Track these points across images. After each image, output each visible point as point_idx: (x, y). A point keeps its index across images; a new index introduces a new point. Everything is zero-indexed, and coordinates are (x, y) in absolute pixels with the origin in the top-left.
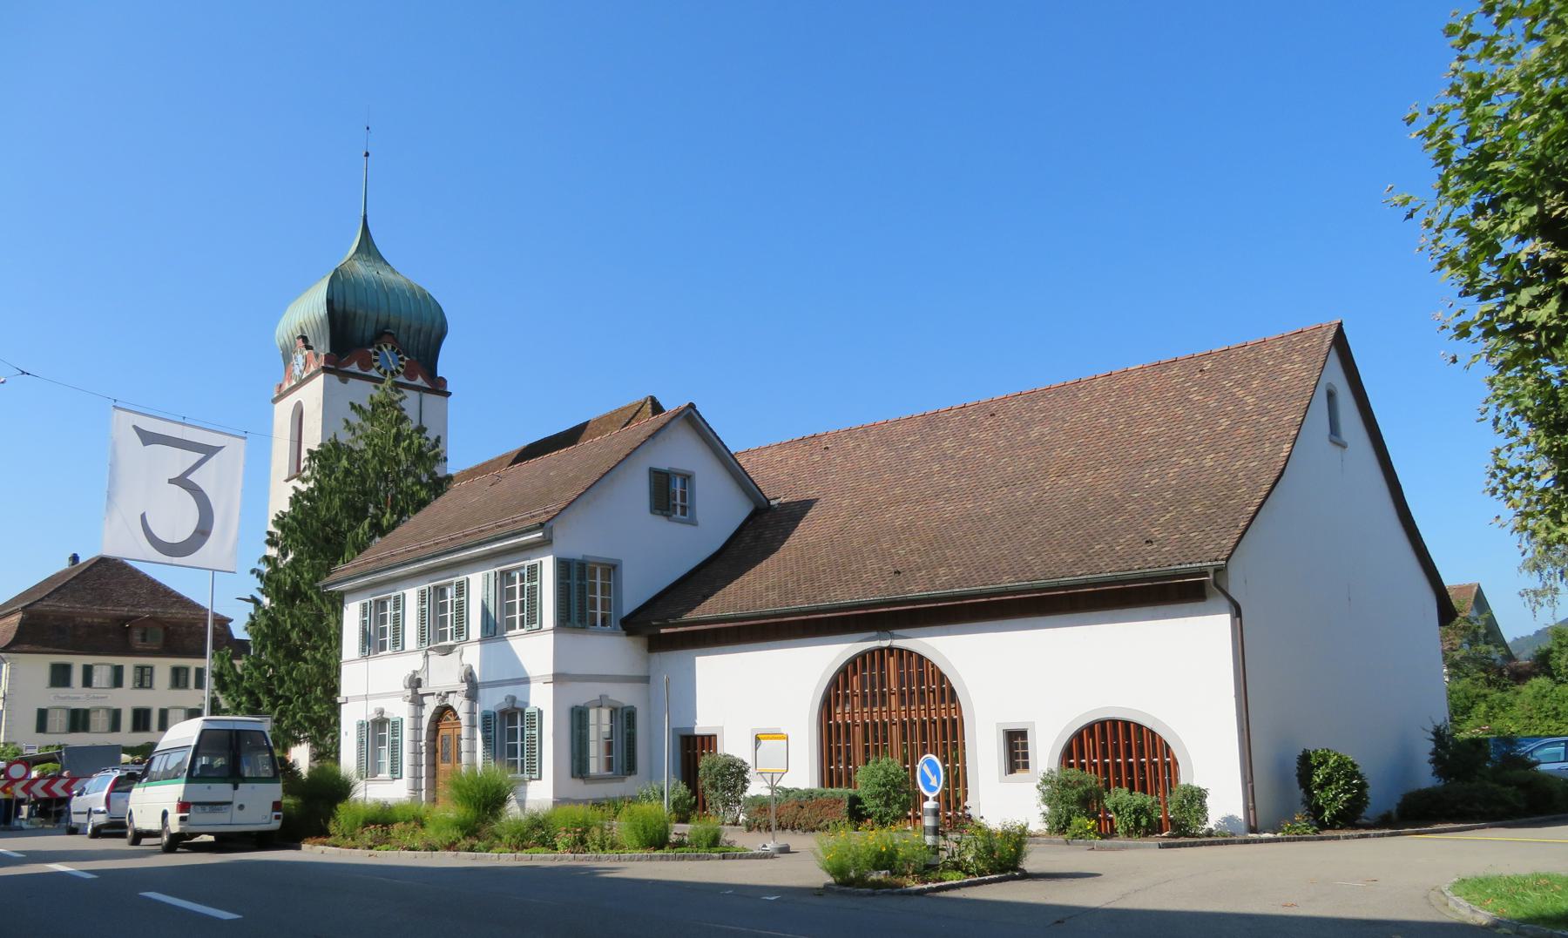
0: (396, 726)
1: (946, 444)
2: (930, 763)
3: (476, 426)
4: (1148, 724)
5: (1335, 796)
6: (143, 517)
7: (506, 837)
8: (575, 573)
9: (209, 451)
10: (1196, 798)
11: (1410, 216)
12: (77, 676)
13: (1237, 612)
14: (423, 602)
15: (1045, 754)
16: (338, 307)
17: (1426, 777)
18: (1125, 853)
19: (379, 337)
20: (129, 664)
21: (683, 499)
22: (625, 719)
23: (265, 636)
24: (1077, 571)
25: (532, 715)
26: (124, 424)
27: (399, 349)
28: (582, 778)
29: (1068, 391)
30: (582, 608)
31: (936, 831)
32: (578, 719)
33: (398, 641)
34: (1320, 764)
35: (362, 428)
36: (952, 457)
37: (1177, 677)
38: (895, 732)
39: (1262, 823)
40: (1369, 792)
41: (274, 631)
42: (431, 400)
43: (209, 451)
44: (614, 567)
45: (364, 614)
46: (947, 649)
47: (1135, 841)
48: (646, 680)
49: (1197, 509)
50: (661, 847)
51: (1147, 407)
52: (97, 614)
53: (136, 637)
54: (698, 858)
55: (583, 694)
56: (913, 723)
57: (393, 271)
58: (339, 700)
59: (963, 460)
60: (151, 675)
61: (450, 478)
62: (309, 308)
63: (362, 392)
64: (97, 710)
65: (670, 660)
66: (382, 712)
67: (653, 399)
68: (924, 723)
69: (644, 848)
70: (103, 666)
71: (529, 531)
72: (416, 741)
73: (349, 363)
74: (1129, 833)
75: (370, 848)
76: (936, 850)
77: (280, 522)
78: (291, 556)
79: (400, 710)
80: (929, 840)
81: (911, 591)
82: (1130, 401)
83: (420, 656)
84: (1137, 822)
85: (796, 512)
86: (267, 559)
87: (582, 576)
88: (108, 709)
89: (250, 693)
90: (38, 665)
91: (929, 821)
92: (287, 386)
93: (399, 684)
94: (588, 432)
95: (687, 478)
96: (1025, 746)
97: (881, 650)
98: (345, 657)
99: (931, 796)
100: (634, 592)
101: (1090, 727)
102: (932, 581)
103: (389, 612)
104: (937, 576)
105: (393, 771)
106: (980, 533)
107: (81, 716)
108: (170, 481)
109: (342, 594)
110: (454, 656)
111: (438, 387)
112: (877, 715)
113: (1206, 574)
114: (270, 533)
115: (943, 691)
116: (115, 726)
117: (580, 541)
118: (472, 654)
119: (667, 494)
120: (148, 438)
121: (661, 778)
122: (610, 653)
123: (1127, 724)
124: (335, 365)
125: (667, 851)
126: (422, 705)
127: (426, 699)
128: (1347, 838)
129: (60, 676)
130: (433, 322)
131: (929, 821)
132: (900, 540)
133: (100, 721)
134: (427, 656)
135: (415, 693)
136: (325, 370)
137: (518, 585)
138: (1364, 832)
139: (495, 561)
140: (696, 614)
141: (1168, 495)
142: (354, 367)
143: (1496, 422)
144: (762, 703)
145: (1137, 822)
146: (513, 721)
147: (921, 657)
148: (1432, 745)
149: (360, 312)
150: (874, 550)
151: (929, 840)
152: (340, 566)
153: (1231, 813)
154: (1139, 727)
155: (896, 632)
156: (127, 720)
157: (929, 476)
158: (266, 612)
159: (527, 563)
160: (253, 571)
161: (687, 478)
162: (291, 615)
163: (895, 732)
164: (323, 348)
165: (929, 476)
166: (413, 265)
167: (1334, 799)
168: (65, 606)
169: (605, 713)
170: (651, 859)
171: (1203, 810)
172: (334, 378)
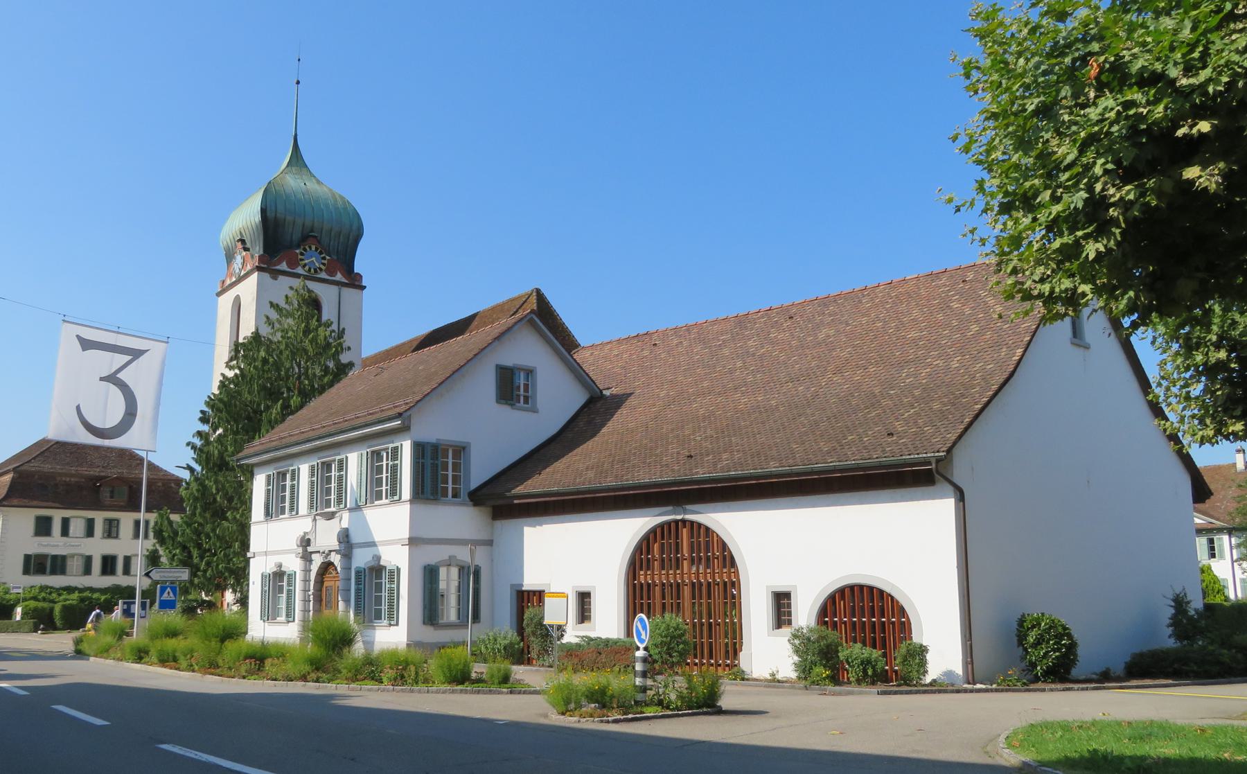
0: (291, 577)
1: (750, 343)
2: (641, 620)
3: (386, 313)
4: (887, 589)
5: (1046, 654)
6: (78, 408)
7: (344, 671)
8: (428, 453)
9: (136, 354)
10: (920, 652)
11: (958, 210)
12: (57, 527)
13: (960, 496)
14: (313, 475)
15: (805, 614)
16: (270, 214)
17: (1167, 641)
18: (850, 698)
19: (304, 241)
20: (99, 517)
21: (526, 390)
22: (471, 575)
23: (196, 499)
24: (828, 460)
25: (391, 572)
26: (68, 334)
27: (322, 250)
28: (432, 624)
29: (854, 297)
31: (644, 675)
32: (430, 574)
33: (294, 507)
34: (1034, 626)
35: (280, 322)
36: (753, 355)
37: (907, 548)
38: (687, 591)
40: (1081, 651)
41: (203, 494)
42: (347, 292)
43: (136, 354)
44: (464, 448)
45: (268, 484)
46: (733, 524)
47: (864, 688)
48: (490, 543)
49: (936, 406)
50: (462, 683)
51: (915, 313)
52: (67, 478)
53: (105, 494)
54: (490, 692)
55: (434, 555)
56: (701, 584)
57: (318, 182)
59: (761, 356)
60: (118, 526)
61: (351, 365)
62: (246, 216)
63: (284, 288)
64: (73, 556)
65: (506, 527)
66: (280, 566)
67: (538, 291)
68: (709, 584)
69: (449, 683)
70: (78, 518)
71: (390, 419)
72: (305, 591)
73: (280, 262)
74: (859, 682)
75: (244, 677)
76: (644, 689)
77: (211, 403)
78: (220, 431)
79: (293, 564)
80: (638, 681)
81: (697, 473)
82: (903, 307)
83: (310, 520)
84: (865, 671)
85: (618, 402)
86: (199, 434)
88: (82, 555)
89: (184, 548)
90: (25, 518)
91: (639, 667)
92: (228, 282)
93: (293, 543)
94: (475, 323)
95: (530, 372)
96: (789, 606)
97: (677, 522)
98: (253, 519)
99: (642, 646)
100: (480, 471)
101: (841, 591)
102: (715, 464)
103: (334, 473)
104: (720, 460)
105: (287, 616)
106: (763, 423)
107: (59, 562)
108: (102, 379)
109: (253, 465)
110: (335, 521)
111: (355, 282)
112: (672, 576)
113: (929, 463)
114: (202, 412)
115: (724, 557)
116: (87, 571)
117: (435, 426)
118: (345, 520)
119: (512, 386)
120: (86, 344)
121: (499, 623)
122: (459, 520)
123: (871, 589)
124: (267, 266)
125: (467, 686)
126: (311, 561)
127: (314, 556)
128: (1052, 690)
129: (43, 527)
130: (351, 226)
131: (639, 667)
132: (699, 428)
133: (75, 565)
134: (315, 520)
135: (305, 551)
136: (259, 269)
137: (384, 463)
138: (1071, 686)
139: (367, 443)
140: (520, 490)
141: (917, 393)
142: (284, 266)
143: (1153, 343)
144: (579, 563)
145: (865, 671)
146: (379, 576)
147: (707, 529)
148: (1173, 611)
149: (289, 218)
150: (678, 436)
151: (638, 681)
152: (256, 442)
153: (950, 668)
154: (881, 592)
155: (689, 507)
156: (97, 565)
157: (731, 372)
158: (197, 479)
159: (391, 446)
160: (188, 444)
161: (530, 372)
162: (216, 482)
163: (687, 591)
164: (258, 250)
165: (731, 372)
166: (334, 179)
167: (1047, 655)
168: (47, 467)
169: (454, 571)
170: (453, 692)
171: (923, 663)
172: (266, 276)
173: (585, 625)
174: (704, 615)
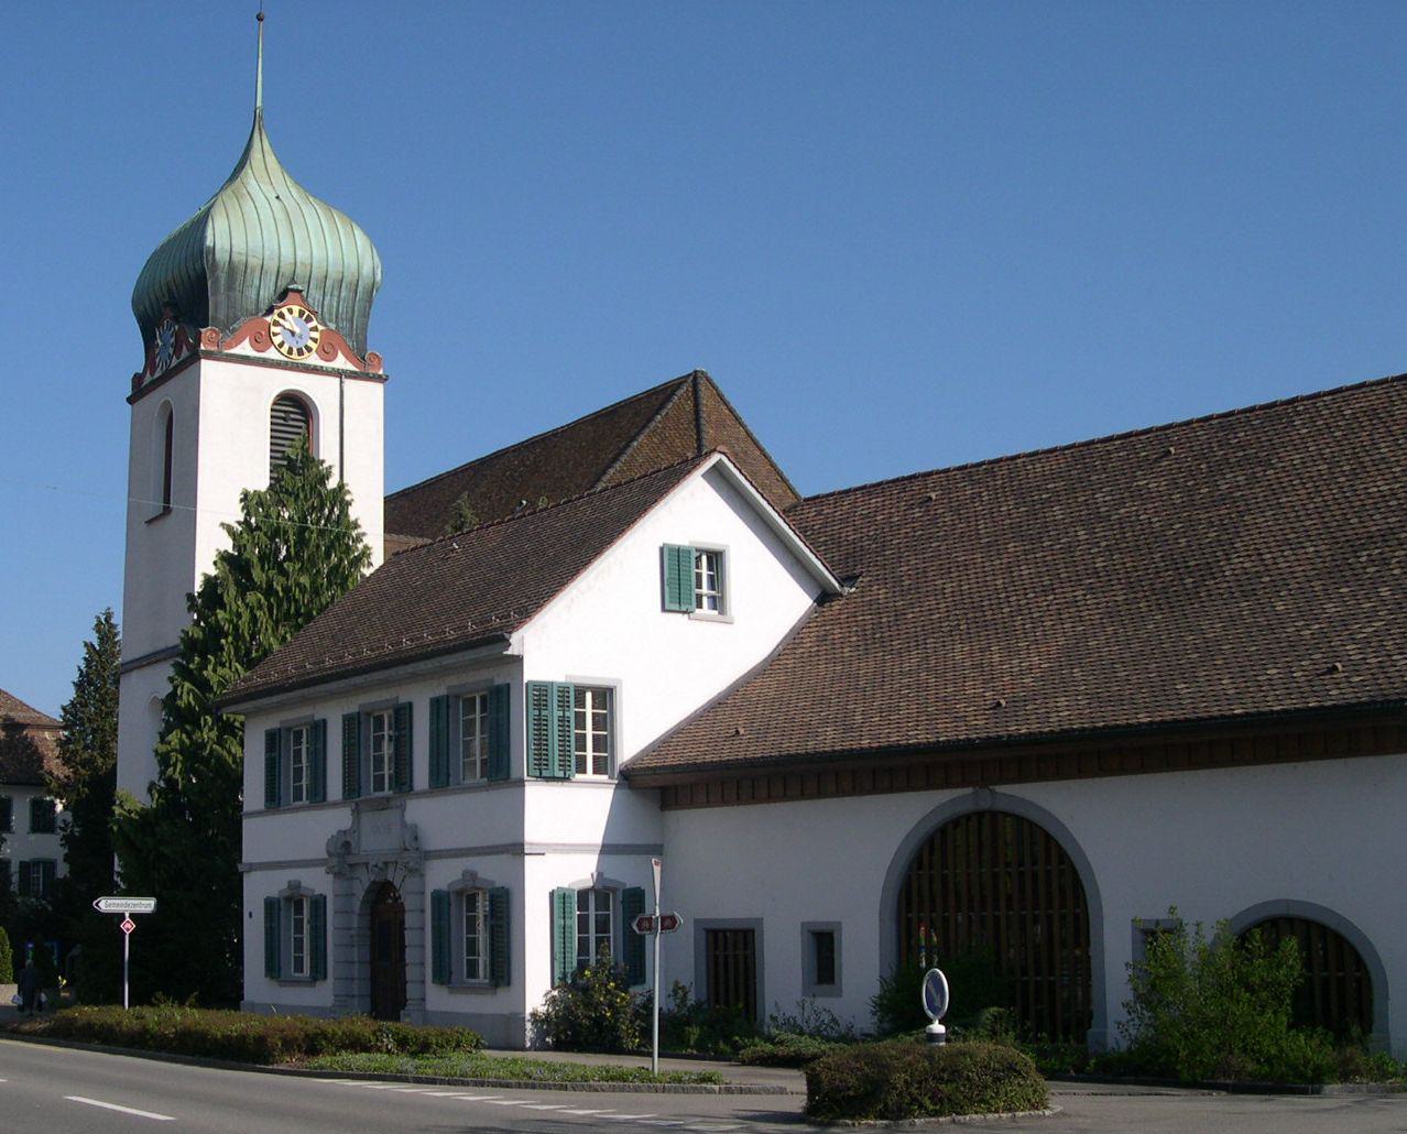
0: (319, 904)
30: (565, 753)
39: (541, 1046)
48: (657, 850)
58: (240, 868)
60: (753, 935)
79: (318, 882)
87: (564, 705)
95: (715, 558)
110: (391, 816)
149: (254, 262)
161: (715, 558)
165: (1069, 548)
173: (501, 992)
174: (741, 946)
